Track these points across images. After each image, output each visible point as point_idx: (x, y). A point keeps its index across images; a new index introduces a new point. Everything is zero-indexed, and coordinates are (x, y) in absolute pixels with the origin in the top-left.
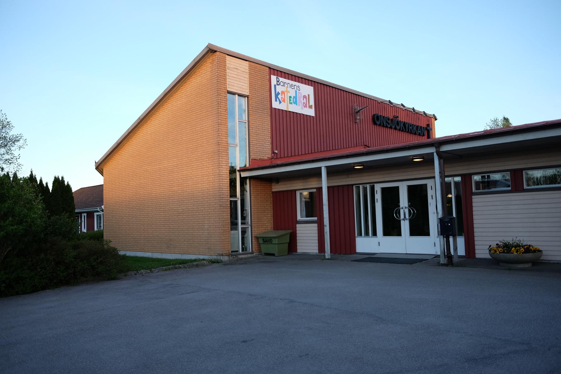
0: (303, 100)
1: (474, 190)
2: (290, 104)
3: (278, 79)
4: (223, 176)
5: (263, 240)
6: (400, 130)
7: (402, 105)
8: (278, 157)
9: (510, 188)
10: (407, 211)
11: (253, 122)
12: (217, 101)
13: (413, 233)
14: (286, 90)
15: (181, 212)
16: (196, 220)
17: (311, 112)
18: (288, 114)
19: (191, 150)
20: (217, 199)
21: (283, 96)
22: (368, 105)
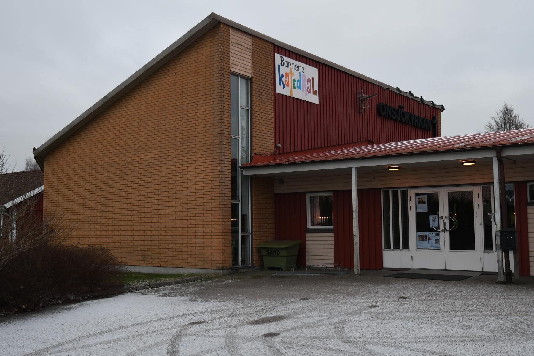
0: (308, 84)
2: (294, 88)
3: (282, 58)
4: (225, 173)
7: (411, 94)
8: (281, 152)
10: (447, 221)
13: (455, 245)
14: (290, 72)
15: (164, 216)
16: (186, 226)
17: (314, 99)
19: (181, 140)
20: (216, 201)
22: (377, 93)
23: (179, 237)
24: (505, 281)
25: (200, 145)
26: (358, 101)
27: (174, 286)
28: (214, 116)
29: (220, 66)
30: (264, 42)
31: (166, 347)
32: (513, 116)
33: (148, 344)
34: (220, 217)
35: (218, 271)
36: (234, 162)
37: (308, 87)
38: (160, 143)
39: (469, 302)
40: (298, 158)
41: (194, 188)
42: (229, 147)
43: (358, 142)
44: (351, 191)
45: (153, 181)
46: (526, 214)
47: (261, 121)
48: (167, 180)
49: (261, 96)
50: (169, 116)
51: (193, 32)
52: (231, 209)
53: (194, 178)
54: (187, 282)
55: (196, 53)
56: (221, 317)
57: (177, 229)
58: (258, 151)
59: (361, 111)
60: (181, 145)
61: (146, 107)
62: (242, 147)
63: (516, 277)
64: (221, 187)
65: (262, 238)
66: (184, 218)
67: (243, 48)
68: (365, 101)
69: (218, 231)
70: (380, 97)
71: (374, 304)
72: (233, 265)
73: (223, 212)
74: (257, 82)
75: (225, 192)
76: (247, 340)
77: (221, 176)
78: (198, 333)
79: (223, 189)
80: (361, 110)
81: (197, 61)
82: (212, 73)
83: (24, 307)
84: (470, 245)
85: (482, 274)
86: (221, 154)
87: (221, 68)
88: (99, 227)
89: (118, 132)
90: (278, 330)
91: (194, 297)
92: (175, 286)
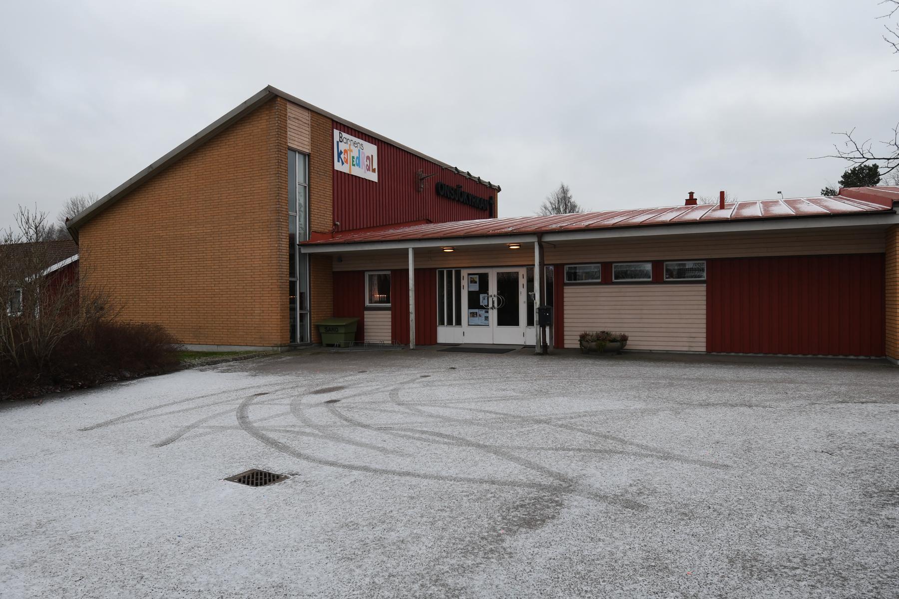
0: (367, 161)
1: (566, 281)
4: (283, 251)
5: (326, 328)
6: (463, 202)
7: (468, 173)
8: (340, 230)
9: (599, 280)
10: (495, 299)
11: (314, 187)
12: (277, 158)
13: (501, 322)
14: (349, 148)
15: (218, 293)
17: (374, 177)
18: (350, 177)
21: (346, 157)
23: (234, 314)
24: (542, 352)
25: (256, 222)
26: (417, 180)
27: (231, 363)
28: (271, 192)
29: (277, 141)
30: (322, 118)
31: (236, 414)
32: (569, 195)
33: (216, 412)
34: (277, 295)
35: (275, 348)
36: (292, 238)
37: (367, 165)
38: (212, 217)
39: (509, 371)
40: (357, 237)
41: (250, 266)
42: (287, 224)
43: (416, 221)
44: (408, 270)
45: (205, 257)
46: (563, 293)
47: (320, 199)
48: (221, 256)
49: (319, 173)
50: (222, 190)
51: (248, 104)
52: (288, 287)
53: (250, 255)
54: (244, 359)
55: (251, 126)
56: (284, 389)
57: (232, 306)
58: (317, 229)
59: (420, 190)
60: (236, 220)
61: (197, 180)
62: (300, 224)
63: (550, 349)
64: (278, 264)
65: (321, 315)
66: (240, 295)
67: (300, 122)
68: (424, 180)
69: (276, 309)
70: (434, 179)
71: (426, 374)
72: (291, 342)
73: (281, 289)
74: (315, 159)
75: (283, 270)
76: (311, 406)
77: (278, 253)
78: (263, 402)
79: (281, 267)
80: (420, 188)
81: (252, 134)
82: (269, 148)
83: (80, 383)
84: (515, 322)
85: (524, 347)
86: (278, 231)
87: (278, 143)
88: (145, 304)
89: (165, 204)
90: (339, 397)
91: (254, 373)
92: (234, 363)
